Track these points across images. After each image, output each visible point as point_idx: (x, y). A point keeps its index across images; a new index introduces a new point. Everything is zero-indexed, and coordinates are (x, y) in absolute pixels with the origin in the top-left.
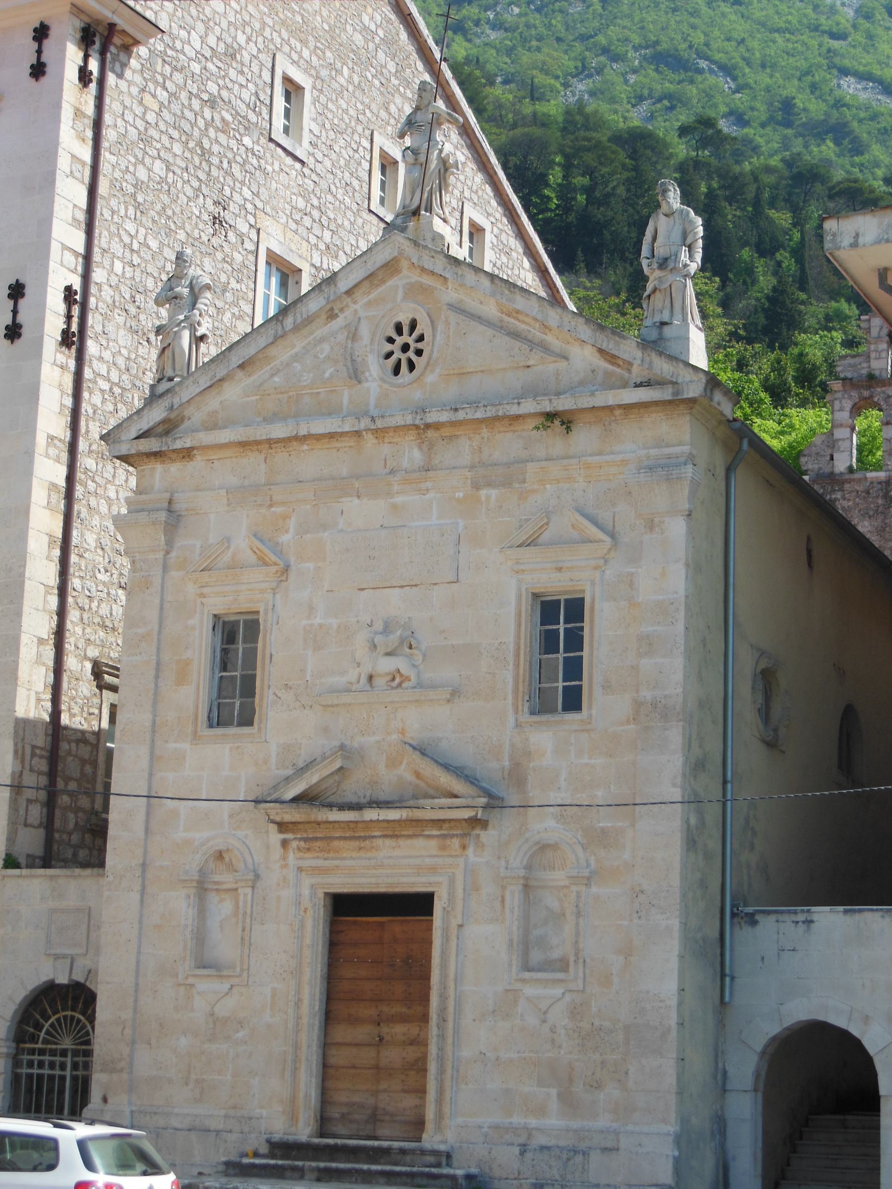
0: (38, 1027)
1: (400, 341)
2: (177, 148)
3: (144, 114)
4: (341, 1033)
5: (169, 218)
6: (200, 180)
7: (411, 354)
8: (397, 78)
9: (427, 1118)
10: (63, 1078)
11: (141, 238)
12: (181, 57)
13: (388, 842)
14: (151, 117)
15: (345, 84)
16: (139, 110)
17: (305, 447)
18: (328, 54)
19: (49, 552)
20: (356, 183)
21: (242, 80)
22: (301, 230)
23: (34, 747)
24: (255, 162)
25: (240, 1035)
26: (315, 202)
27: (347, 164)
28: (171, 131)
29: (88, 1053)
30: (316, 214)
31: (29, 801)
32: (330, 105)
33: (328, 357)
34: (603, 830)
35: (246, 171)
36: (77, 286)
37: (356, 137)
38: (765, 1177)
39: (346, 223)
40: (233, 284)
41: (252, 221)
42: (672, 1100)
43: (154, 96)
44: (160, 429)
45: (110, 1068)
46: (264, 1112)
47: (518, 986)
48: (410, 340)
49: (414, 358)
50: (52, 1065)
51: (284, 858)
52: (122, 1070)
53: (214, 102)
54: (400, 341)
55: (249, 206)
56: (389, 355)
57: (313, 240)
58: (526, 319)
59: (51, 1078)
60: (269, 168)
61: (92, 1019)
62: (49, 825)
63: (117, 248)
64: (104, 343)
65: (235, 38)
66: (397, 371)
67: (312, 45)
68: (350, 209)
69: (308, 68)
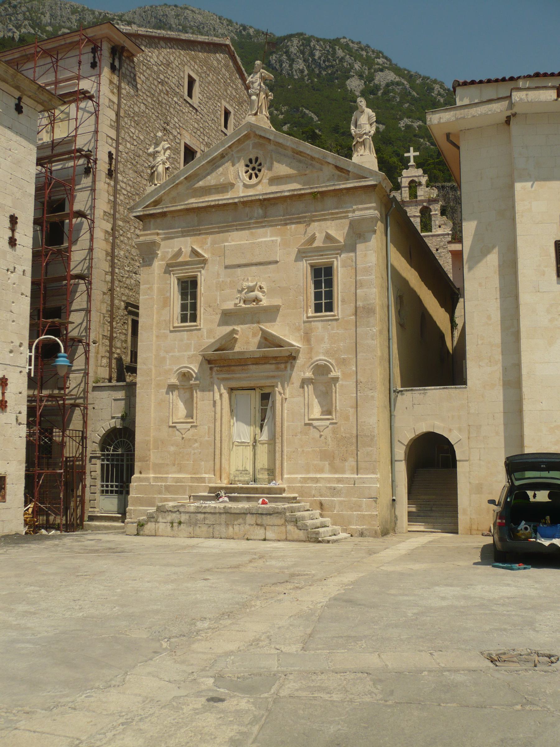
1: (251, 166)
2: (149, 100)
5: (147, 127)
6: (158, 113)
10: (122, 465)
11: (136, 134)
12: (150, 63)
13: (254, 366)
18: (205, 68)
24: (179, 108)
26: (201, 125)
28: (147, 93)
30: (202, 130)
31: (102, 357)
33: (222, 173)
36: (114, 151)
41: (179, 131)
48: (256, 166)
49: (257, 172)
50: (117, 460)
51: (211, 374)
53: (163, 83)
54: (251, 166)
55: (177, 125)
57: (201, 140)
58: (304, 155)
65: (169, 58)
66: (250, 178)
69: (197, 73)
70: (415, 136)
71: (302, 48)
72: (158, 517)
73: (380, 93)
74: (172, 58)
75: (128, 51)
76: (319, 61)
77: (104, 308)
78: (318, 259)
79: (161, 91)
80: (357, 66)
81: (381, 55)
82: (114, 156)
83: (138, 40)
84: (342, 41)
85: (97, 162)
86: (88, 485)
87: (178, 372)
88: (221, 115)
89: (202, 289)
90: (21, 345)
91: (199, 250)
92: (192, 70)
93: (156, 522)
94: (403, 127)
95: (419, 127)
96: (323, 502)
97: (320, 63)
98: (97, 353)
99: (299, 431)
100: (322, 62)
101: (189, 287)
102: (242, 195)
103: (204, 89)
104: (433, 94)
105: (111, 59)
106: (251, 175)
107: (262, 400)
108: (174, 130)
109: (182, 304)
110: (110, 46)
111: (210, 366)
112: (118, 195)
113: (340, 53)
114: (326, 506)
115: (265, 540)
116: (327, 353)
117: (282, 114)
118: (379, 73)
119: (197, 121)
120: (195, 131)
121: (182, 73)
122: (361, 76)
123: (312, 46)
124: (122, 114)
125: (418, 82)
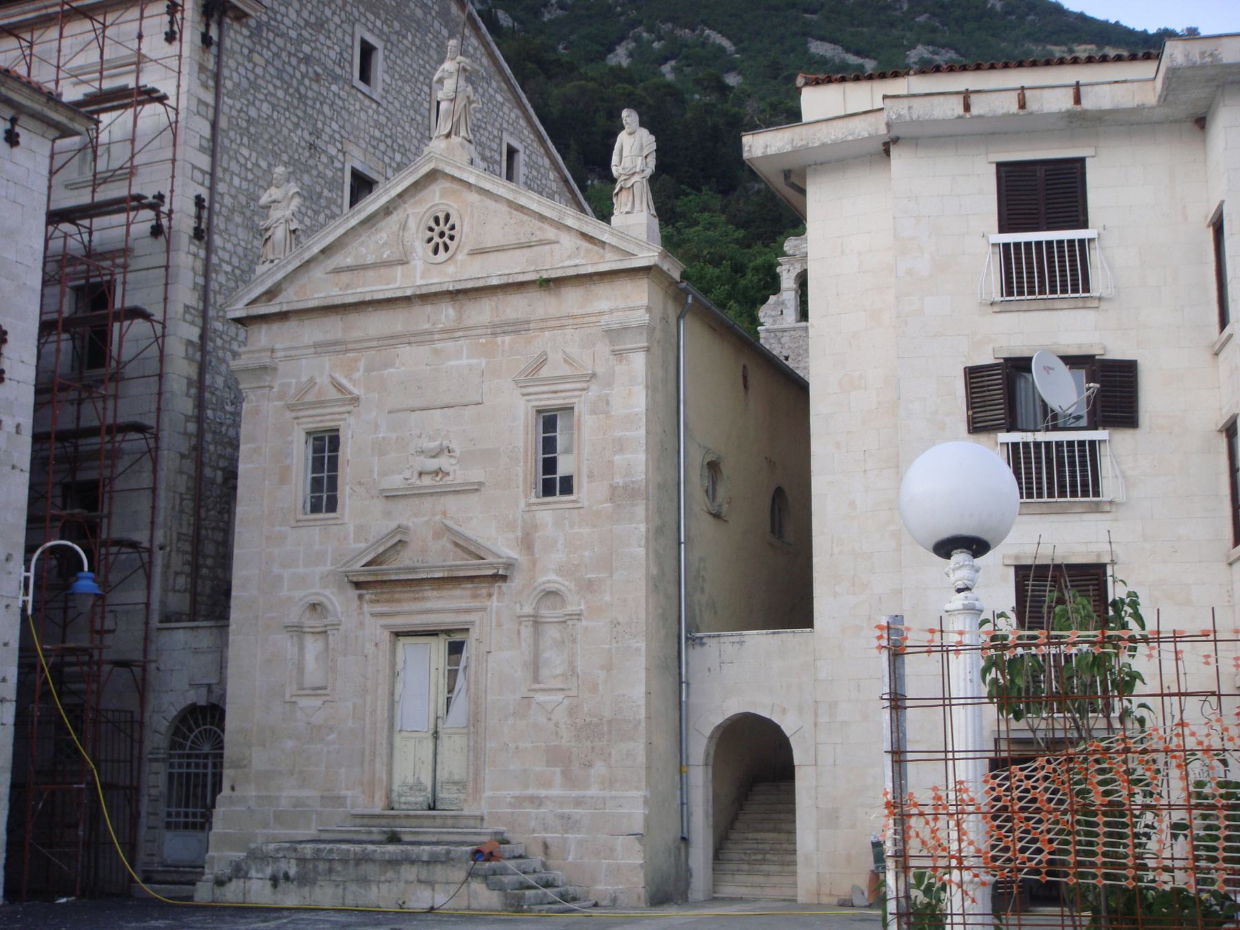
0: (186, 738)
2: (280, 94)
5: (274, 145)
6: (298, 117)
7: (446, 239)
10: (205, 775)
11: (253, 159)
14: (259, 71)
18: (396, 23)
20: (419, 118)
21: (329, 43)
24: (340, 103)
26: (388, 132)
27: (413, 103)
29: (221, 756)
30: (389, 141)
31: (177, 574)
32: (398, 61)
33: (385, 243)
34: (590, 581)
36: (205, 194)
37: (419, 85)
38: (715, 826)
39: (412, 148)
40: (326, 193)
42: (643, 773)
43: (261, 55)
45: (237, 765)
46: (349, 793)
47: (531, 694)
48: (446, 229)
49: (448, 241)
50: (197, 766)
51: (360, 608)
55: (337, 136)
56: (430, 240)
57: (387, 160)
59: (197, 775)
60: (352, 108)
61: (223, 730)
63: (234, 167)
65: (323, 12)
66: (436, 251)
67: (383, 16)
69: (380, 35)
72: (249, 869)
74: (328, 12)
77: (182, 483)
79: (304, 76)
82: (206, 204)
85: (173, 216)
86: (144, 814)
88: (429, 110)
89: (347, 451)
90: (8, 558)
91: (344, 381)
92: (369, 30)
93: (246, 877)
94: (915, 63)
96: (549, 841)
98: (167, 566)
101: (326, 448)
102: (419, 282)
103: (395, 63)
107: (450, 654)
109: (313, 479)
112: (214, 275)
114: (553, 850)
116: (560, 571)
117: (660, 39)
120: (374, 143)
124: (223, 123)
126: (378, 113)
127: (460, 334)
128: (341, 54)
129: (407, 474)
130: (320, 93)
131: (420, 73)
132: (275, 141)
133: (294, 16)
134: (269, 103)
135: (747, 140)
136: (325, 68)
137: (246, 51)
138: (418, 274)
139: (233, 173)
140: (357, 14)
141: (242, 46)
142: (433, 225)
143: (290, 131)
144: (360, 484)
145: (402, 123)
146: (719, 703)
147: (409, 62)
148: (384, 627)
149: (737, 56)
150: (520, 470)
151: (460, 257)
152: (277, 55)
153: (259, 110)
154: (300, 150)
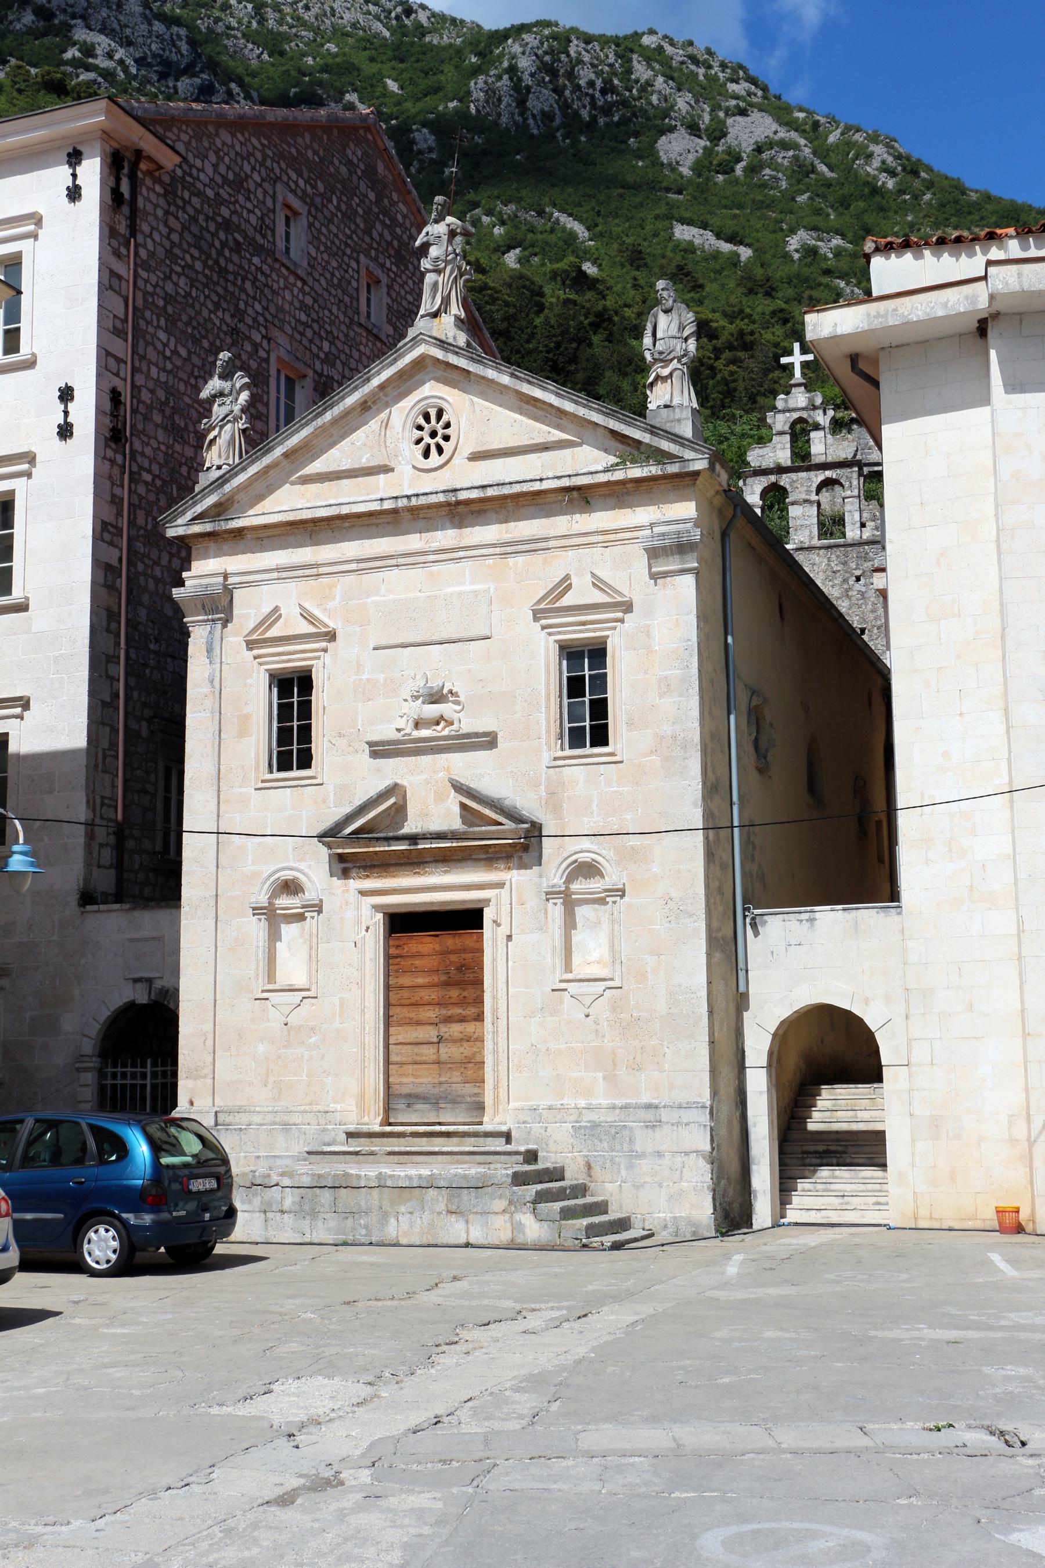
2: (198, 266)
3: (169, 234)
4: (399, 1034)
7: (439, 439)
8: (377, 206)
9: (486, 1104)
11: (172, 345)
14: (175, 237)
15: (334, 211)
16: (164, 230)
17: (347, 524)
18: (320, 184)
19: (109, 624)
22: (305, 341)
23: (103, 797)
24: (263, 279)
25: (313, 1040)
26: (314, 316)
30: (316, 327)
31: (101, 845)
32: (324, 230)
34: (633, 848)
35: (257, 288)
37: (346, 259)
39: (341, 335)
43: (177, 218)
44: (213, 512)
47: (563, 985)
49: (442, 443)
50: (134, 1076)
52: (205, 1076)
55: (261, 319)
57: (315, 350)
60: (275, 287)
62: (119, 866)
64: (145, 439)
65: (241, 168)
66: (426, 454)
67: (306, 174)
68: (344, 323)
69: (303, 197)
70: (828, 272)
71: (547, 58)
73: (739, 168)
74: (247, 168)
75: (149, 158)
76: (591, 91)
78: (575, 632)
79: (224, 244)
80: (683, 103)
81: (741, 73)
83: (170, 131)
84: (646, 40)
87: (272, 879)
88: (357, 290)
89: (319, 698)
91: (317, 613)
92: (291, 191)
94: (797, 251)
95: (838, 253)
97: (592, 97)
99: (540, 1006)
100: (597, 94)
101: (294, 690)
103: (319, 231)
104: (868, 169)
105: (112, 178)
106: (428, 447)
108: (252, 331)
110: (108, 150)
111: (343, 865)
113: (641, 71)
115: (382, 500)
118: (738, 118)
119: (304, 307)
120: (301, 328)
121: (269, 202)
122: (694, 129)
123: (573, 54)
125: (832, 139)
126: (304, 294)
127: (461, 554)
128: (262, 219)
129: (401, 723)
130: (241, 267)
131: (347, 245)
132: (195, 323)
133: (210, 171)
134: (187, 277)
135: (810, 319)
136: (246, 237)
137: (160, 213)
138: (406, 483)
139: (150, 362)
140: (277, 171)
141: (156, 206)
142: (421, 421)
143: (211, 312)
144: (340, 735)
145: (329, 304)
146: (776, 995)
147: (335, 230)
148: (376, 908)
149: (591, 243)
150: (542, 717)
151: (460, 460)
152: (193, 219)
153: (176, 285)
154: (222, 335)
